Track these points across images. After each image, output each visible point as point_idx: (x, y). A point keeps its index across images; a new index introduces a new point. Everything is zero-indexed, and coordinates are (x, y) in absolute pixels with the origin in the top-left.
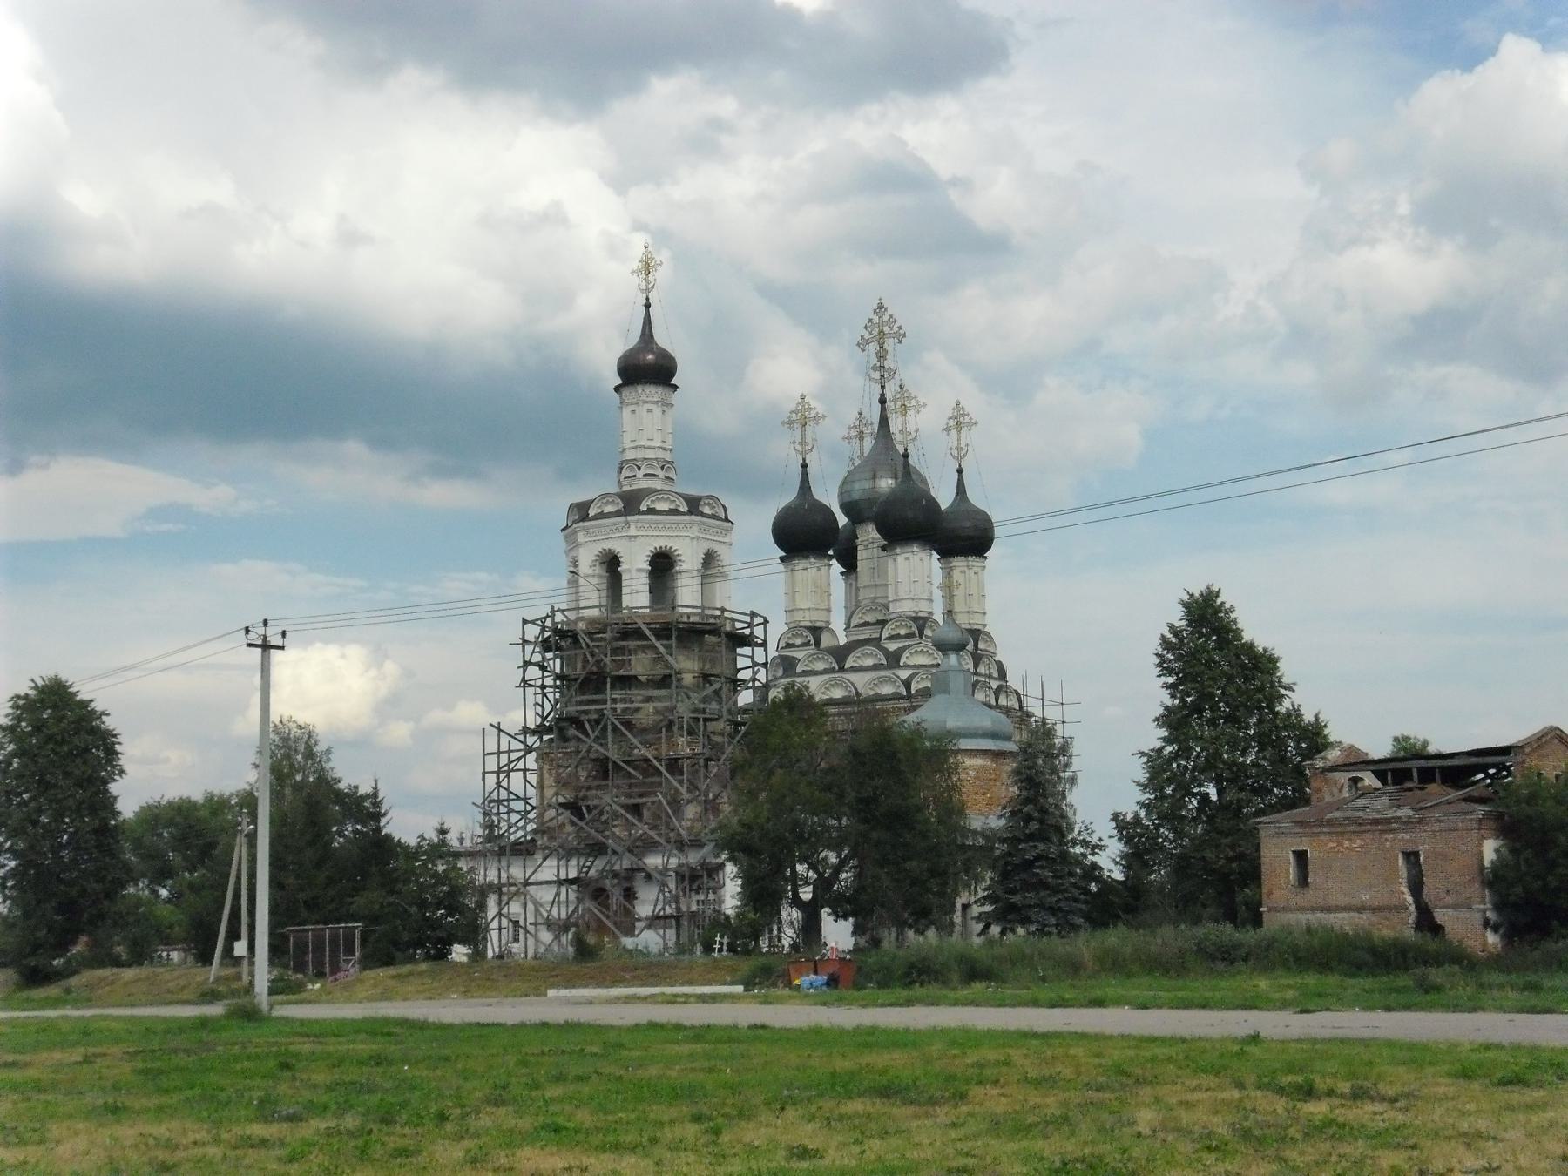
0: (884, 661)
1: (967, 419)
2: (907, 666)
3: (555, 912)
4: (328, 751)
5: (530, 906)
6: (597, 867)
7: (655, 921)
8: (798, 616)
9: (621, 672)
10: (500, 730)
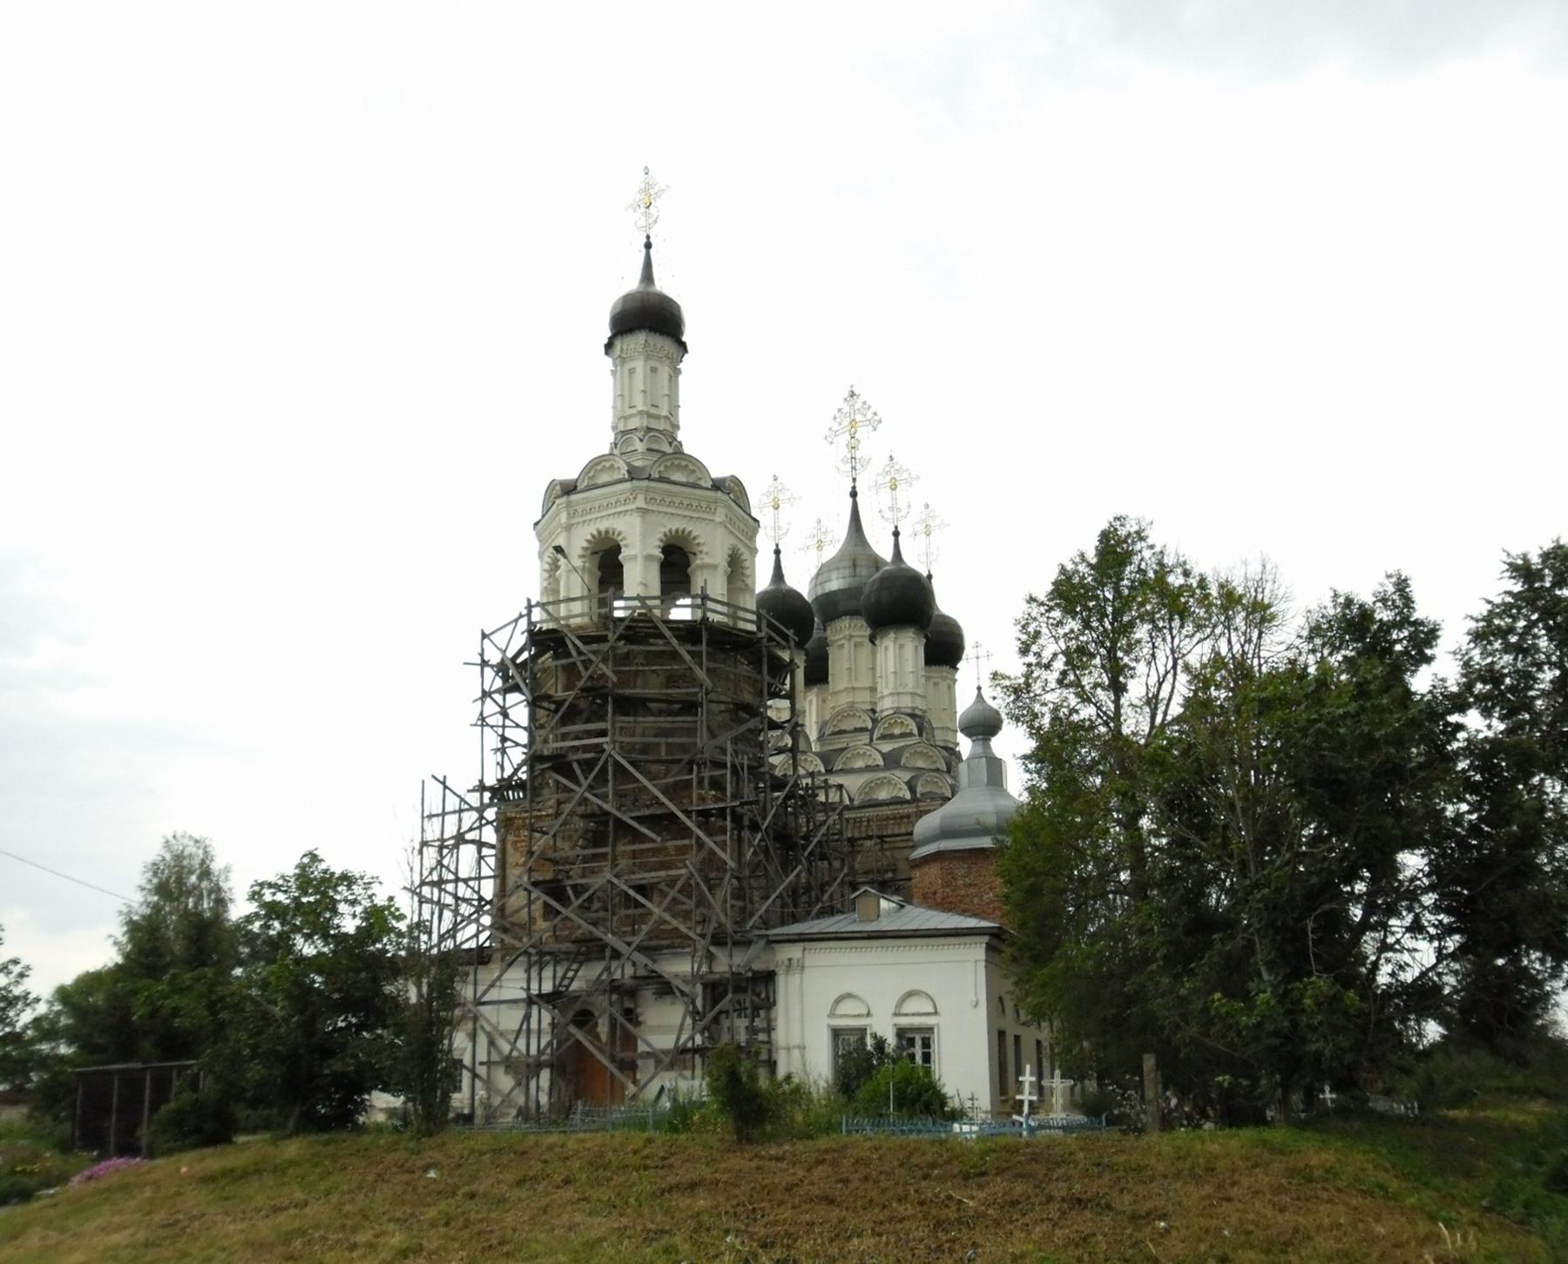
0: (881, 763)
1: (938, 521)
2: (906, 768)
3: (521, 1044)
4: (227, 870)
5: (482, 1040)
6: (583, 978)
7: (680, 1057)
9: (628, 692)
10: (446, 787)
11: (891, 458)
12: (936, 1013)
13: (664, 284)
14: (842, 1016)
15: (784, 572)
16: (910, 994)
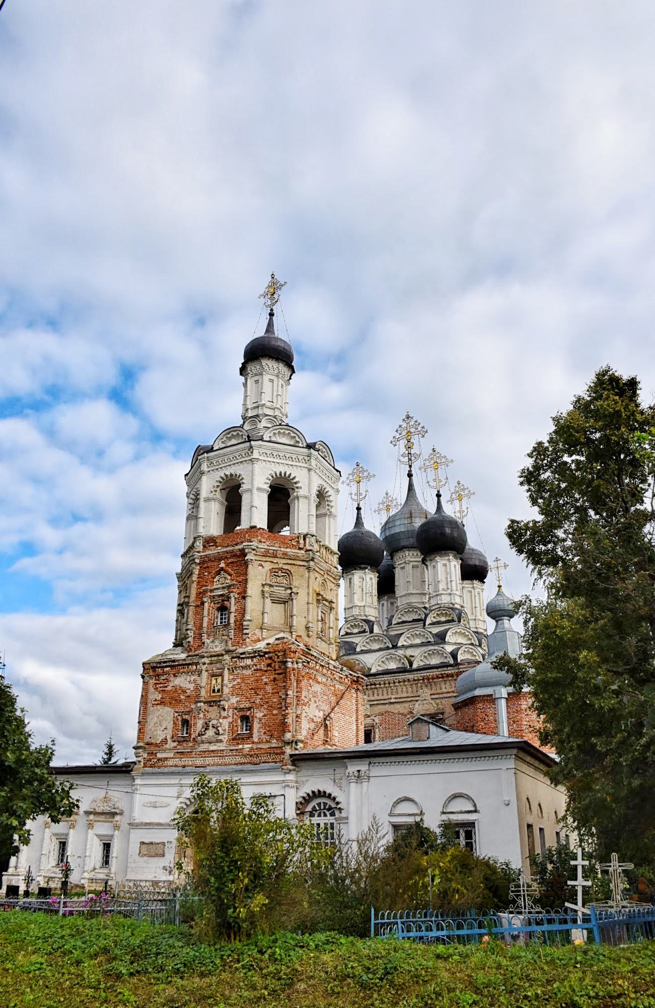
2: (449, 643)
8: (356, 612)
11: (434, 450)
12: (476, 811)
13: (281, 333)
14: (400, 815)
15: (364, 520)
16: (455, 796)
